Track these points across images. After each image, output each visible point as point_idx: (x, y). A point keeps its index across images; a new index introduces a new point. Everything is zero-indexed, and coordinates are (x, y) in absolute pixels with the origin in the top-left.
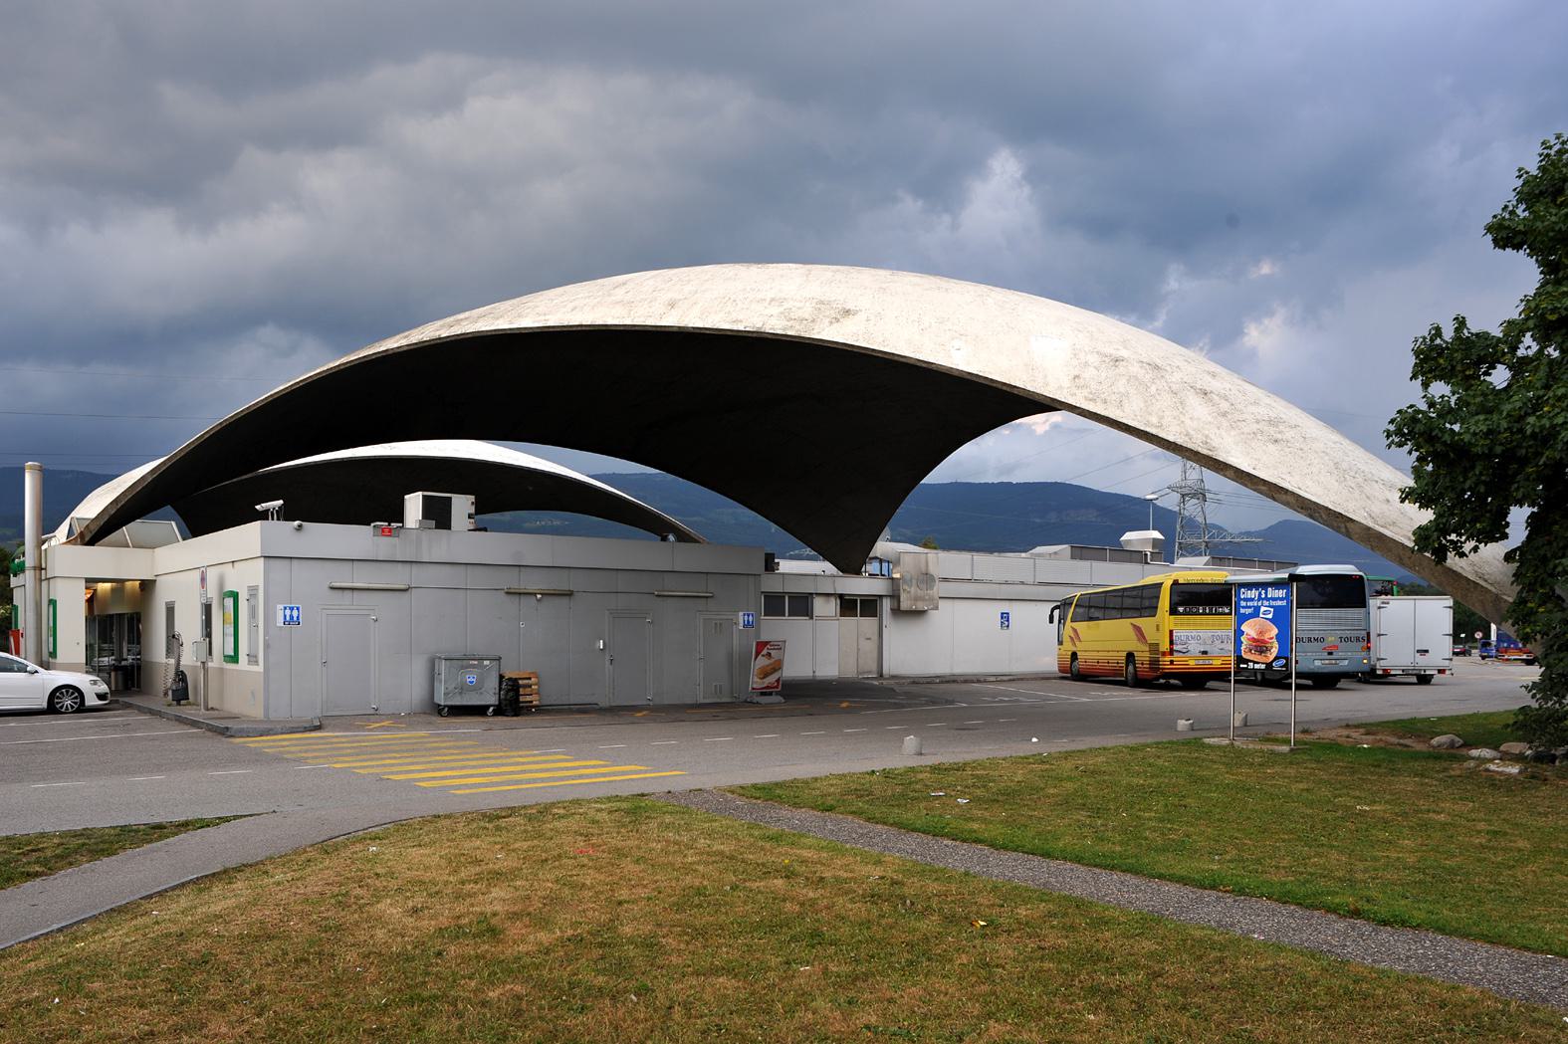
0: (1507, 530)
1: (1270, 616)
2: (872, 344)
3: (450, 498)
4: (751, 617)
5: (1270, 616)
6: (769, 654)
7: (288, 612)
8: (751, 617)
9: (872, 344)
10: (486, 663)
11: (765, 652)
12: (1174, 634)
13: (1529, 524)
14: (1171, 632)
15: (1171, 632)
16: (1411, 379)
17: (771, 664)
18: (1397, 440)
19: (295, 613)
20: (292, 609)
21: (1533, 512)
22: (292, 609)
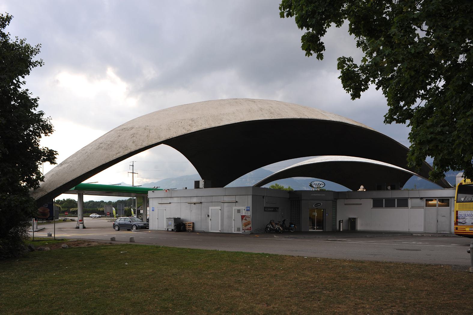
0: (366, 90)
1: (47, 206)
2: (325, 160)
3: (449, 199)
4: (249, 208)
5: (47, 206)
6: (246, 219)
7: (247, 208)
8: (249, 208)
9: (325, 160)
10: (172, 219)
11: (244, 218)
12: (459, 213)
13: (297, 23)
14: (457, 212)
15: (457, 212)
16: (407, 126)
17: (246, 223)
18: (7, 22)
19: (249, 208)
20: (248, 207)
21: (296, 18)
22: (248, 207)
